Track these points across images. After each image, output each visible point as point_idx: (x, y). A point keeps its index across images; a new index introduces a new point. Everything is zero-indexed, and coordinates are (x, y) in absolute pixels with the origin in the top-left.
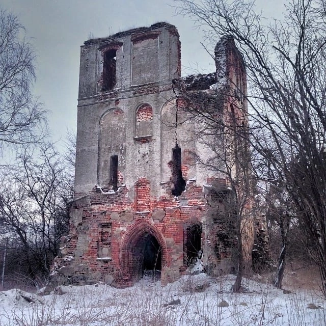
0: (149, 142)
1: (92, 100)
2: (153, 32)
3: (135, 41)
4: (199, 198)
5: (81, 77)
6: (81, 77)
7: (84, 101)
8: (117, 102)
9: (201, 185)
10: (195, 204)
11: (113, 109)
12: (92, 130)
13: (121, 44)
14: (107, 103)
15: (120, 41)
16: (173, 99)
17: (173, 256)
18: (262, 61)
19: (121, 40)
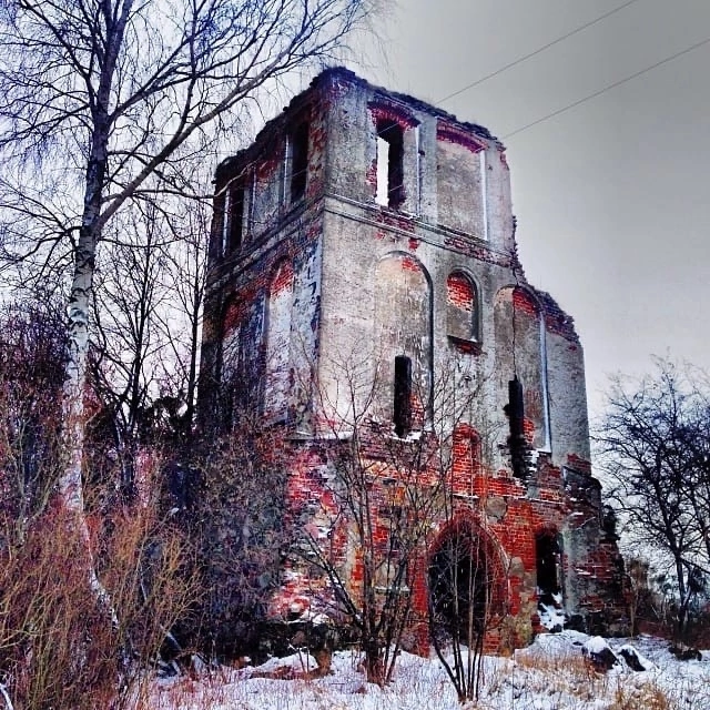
0: (475, 355)
1: (360, 210)
2: (476, 138)
3: (441, 134)
4: (557, 488)
5: (582, 398)
6: (582, 398)
7: (340, 205)
8: (414, 243)
9: (559, 465)
10: (549, 497)
11: (401, 252)
12: (359, 281)
13: (415, 123)
14: (393, 235)
15: (417, 117)
16: (510, 286)
17: (521, 594)
18: (350, 203)
19: (419, 115)
